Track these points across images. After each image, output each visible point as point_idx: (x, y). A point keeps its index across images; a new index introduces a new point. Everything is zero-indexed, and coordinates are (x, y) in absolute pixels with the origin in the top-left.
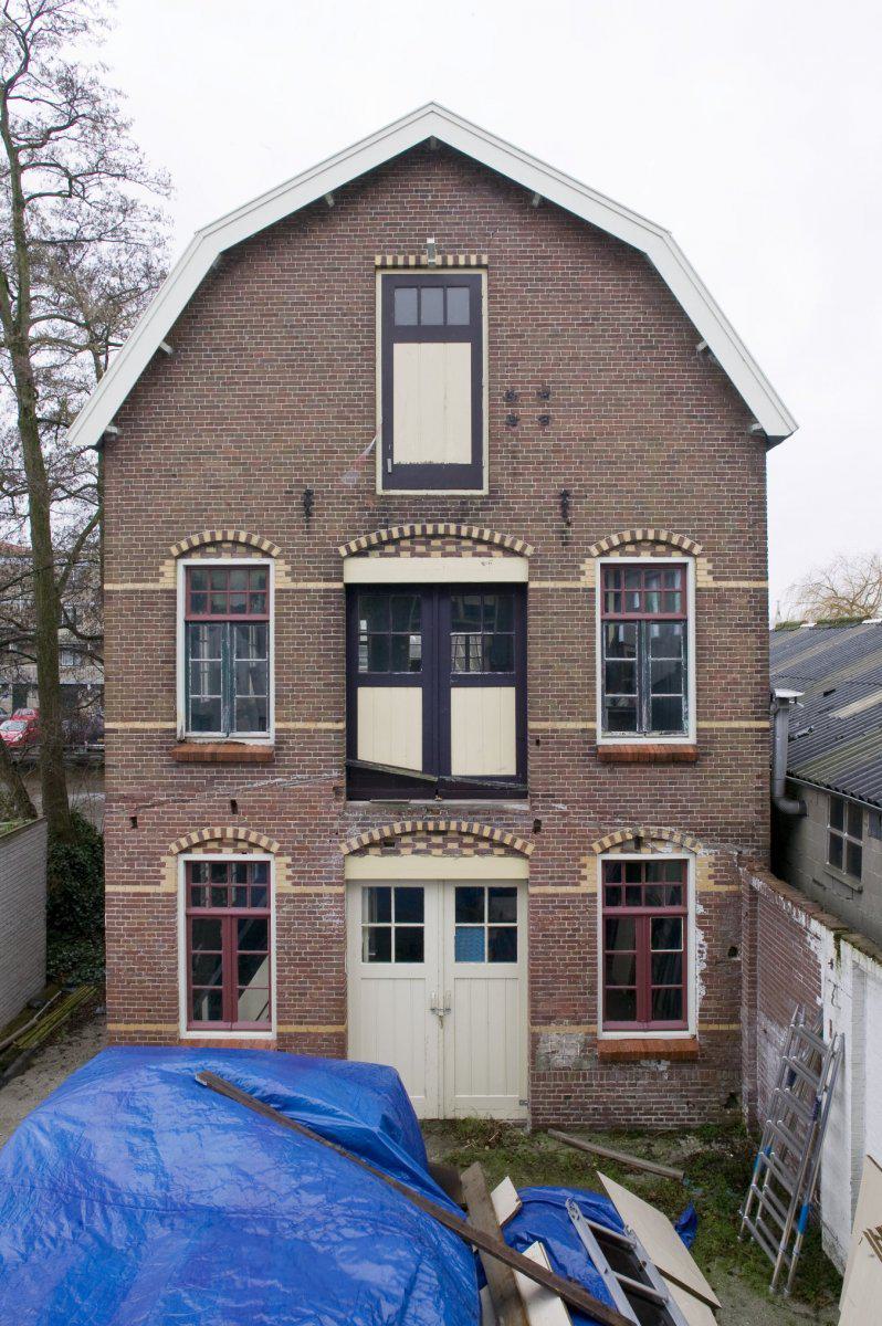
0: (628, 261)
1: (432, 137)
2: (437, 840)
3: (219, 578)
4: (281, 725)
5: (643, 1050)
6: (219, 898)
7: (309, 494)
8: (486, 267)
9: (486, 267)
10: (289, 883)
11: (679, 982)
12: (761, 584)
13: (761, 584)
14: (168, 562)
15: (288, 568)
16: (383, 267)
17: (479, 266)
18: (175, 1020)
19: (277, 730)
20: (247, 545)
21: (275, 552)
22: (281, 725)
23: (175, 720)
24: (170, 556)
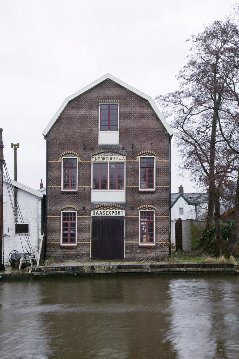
0: (147, 101)
1: (108, 78)
2: (108, 208)
3: (69, 160)
4: (78, 242)
5: (197, 71)
6: (68, 220)
7: (84, 145)
8: (119, 102)
9: (119, 102)
10: (80, 160)
11: (153, 237)
12: (152, 232)
13: (152, 232)
14: (60, 157)
15: (80, 158)
16: (100, 102)
17: (118, 102)
18: (60, 241)
19: (77, 243)
20: (74, 209)
21: (78, 155)
22: (78, 242)
23: (61, 186)
24: (61, 156)
